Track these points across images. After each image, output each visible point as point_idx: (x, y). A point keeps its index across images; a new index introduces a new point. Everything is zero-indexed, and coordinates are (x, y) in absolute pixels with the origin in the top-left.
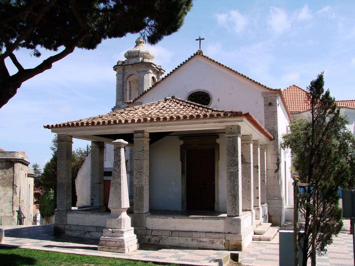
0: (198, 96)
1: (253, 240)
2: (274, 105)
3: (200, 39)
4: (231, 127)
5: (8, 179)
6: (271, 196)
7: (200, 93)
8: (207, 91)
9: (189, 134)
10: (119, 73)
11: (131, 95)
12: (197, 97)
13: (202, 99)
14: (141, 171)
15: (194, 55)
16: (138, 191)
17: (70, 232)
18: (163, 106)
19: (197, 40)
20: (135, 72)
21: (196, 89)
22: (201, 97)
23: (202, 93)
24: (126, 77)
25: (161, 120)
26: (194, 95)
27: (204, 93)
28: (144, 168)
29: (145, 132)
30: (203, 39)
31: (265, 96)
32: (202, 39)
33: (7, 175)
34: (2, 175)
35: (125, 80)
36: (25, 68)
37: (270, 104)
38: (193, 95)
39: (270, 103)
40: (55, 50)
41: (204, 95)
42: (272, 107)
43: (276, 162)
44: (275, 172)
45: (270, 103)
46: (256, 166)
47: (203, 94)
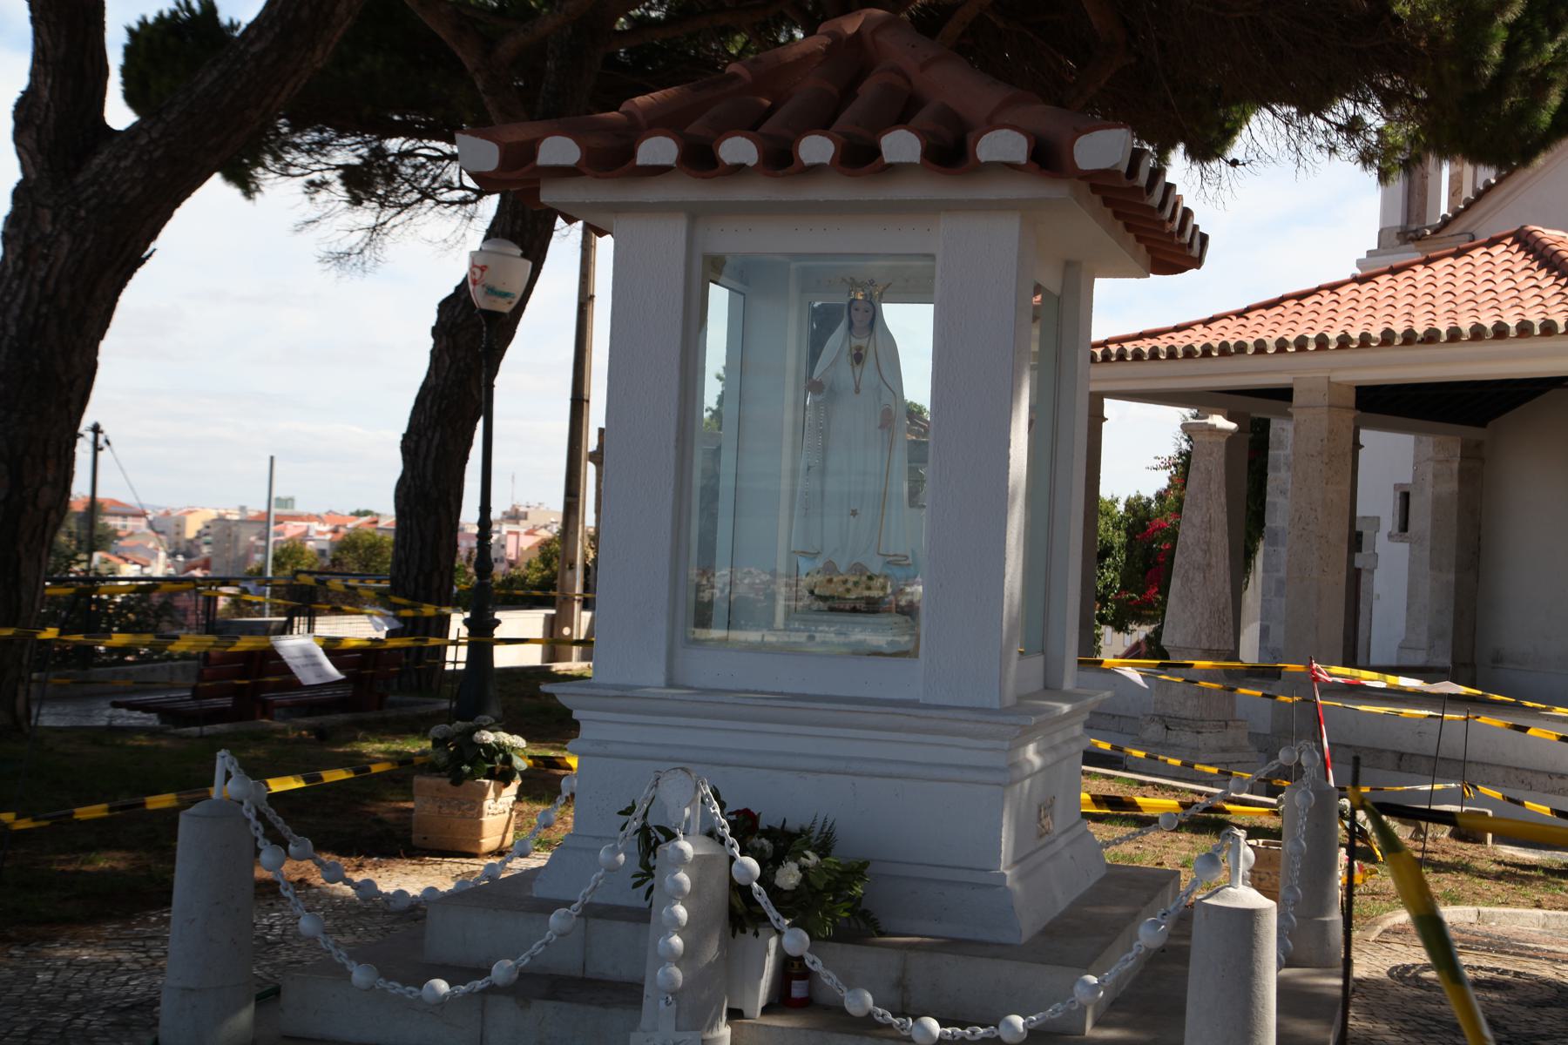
25: (1331, 347)
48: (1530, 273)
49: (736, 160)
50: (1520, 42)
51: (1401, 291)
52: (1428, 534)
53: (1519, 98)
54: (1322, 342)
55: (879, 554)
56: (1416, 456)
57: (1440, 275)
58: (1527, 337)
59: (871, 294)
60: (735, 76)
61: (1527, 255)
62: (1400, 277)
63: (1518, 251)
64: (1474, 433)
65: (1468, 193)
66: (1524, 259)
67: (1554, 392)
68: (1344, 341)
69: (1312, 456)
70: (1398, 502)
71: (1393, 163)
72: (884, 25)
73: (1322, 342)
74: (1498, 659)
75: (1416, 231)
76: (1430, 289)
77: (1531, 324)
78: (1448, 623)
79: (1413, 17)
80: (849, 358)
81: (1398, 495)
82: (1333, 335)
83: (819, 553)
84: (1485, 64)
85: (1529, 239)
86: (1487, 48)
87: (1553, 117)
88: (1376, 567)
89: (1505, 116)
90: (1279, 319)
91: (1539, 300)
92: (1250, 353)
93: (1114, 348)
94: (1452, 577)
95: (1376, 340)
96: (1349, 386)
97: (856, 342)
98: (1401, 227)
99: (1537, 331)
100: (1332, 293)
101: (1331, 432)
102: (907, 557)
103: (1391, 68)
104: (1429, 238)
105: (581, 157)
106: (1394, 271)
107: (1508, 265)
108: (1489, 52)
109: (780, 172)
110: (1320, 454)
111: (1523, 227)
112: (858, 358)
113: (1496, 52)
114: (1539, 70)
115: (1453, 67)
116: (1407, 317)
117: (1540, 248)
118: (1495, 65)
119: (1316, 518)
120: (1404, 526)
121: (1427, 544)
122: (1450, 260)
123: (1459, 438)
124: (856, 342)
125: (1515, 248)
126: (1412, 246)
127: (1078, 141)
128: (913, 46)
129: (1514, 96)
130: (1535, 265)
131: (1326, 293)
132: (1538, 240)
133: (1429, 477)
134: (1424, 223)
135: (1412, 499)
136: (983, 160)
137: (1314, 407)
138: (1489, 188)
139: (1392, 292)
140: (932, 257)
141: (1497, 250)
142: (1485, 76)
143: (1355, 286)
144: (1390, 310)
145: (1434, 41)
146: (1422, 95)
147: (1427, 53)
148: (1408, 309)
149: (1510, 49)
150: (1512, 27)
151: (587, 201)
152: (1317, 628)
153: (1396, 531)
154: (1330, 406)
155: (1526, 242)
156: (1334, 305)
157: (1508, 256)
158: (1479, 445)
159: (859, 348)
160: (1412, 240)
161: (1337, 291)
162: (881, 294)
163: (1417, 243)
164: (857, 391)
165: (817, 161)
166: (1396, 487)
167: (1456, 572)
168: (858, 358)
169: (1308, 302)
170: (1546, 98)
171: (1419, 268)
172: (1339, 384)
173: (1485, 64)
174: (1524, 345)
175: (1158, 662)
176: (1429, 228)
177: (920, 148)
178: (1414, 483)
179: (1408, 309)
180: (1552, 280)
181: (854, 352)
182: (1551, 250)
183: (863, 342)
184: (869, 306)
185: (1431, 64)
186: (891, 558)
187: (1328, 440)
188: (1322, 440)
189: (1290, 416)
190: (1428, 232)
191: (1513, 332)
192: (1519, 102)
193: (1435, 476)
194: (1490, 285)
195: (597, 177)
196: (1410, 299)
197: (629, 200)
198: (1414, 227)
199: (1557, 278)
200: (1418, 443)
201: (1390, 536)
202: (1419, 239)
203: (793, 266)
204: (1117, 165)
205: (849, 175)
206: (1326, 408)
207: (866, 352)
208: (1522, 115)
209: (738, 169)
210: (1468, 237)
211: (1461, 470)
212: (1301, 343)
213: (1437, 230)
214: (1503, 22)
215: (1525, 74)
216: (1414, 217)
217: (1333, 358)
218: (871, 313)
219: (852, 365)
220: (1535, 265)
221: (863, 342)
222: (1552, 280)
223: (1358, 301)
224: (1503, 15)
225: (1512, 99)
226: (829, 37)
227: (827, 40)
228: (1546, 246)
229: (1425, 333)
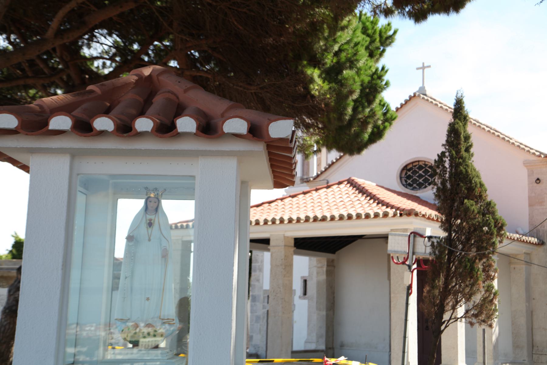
0: (417, 168)
3: (423, 68)
7: (421, 163)
11: (321, 165)
12: (416, 178)
13: (424, 174)
15: (411, 98)
17: (360, 51)
19: (418, 69)
21: (414, 157)
22: (422, 179)
26: (411, 166)
30: (429, 67)
37: (538, 182)
38: (408, 167)
39: (538, 179)
41: (428, 166)
45: (538, 179)
47: (426, 165)
48: (355, 195)
49: (102, 128)
50: (357, 107)
51: (309, 201)
52: (315, 296)
53: (357, 128)
54: (282, 221)
55: (160, 319)
56: (309, 265)
57: (322, 195)
58: (360, 219)
59: (158, 194)
60: (92, 92)
61: (353, 188)
62: (308, 195)
63: (350, 186)
64: (331, 256)
65: (323, 166)
66: (352, 189)
67: (359, 241)
68: (290, 221)
69: (278, 266)
70: (302, 284)
71: (310, 152)
72: (162, 73)
73: (282, 221)
74: (342, 346)
75: (307, 179)
76: (319, 200)
77: (361, 214)
78: (323, 331)
79: (319, 96)
80: (146, 224)
81: (302, 281)
82: (286, 218)
83: (129, 319)
84: (346, 114)
85: (353, 182)
86: (347, 109)
87: (369, 136)
88: (294, 310)
89: (352, 135)
90: (262, 211)
91: (360, 205)
92: (336, 219)
93: (179, 225)
94: (324, 313)
95: (303, 220)
96: (292, 238)
97: (149, 217)
98: (301, 177)
99: (363, 217)
100: (282, 201)
101: (285, 256)
102: (173, 320)
103: (310, 116)
104: (312, 181)
105: (19, 124)
106: (305, 193)
107: (347, 192)
108: (347, 110)
109: (125, 135)
110: (281, 265)
111: (350, 178)
112: (150, 224)
113: (350, 110)
114: (364, 118)
115: (335, 115)
116: (312, 211)
117: (357, 186)
118: (350, 115)
119: (280, 291)
120: (305, 293)
121: (315, 300)
122: (325, 190)
123: (326, 258)
124: (149, 217)
125: (349, 185)
126: (305, 184)
127: (271, 125)
128: (179, 82)
129: (355, 127)
130: (357, 192)
131: (279, 201)
132: (356, 183)
133: (315, 273)
134: (309, 176)
135: (308, 283)
136: (226, 132)
137: (279, 246)
138: (333, 163)
139: (304, 201)
140: (193, 177)
141: (342, 186)
142: (346, 119)
143: (290, 199)
144: (305, 208)
145: (327, 105)
146: (320, 126)
147: (325, 109)
148: (312, 208)
149: (355, 109)
150: (355, 101)
151: (18, 147)
152: (281, 337)
153: (302, 295)
154: (285, 246)
155: (351, 183)
156: (283, 206)
157: (346, 188)
158: (333, 261)
159: (151, 220)
160: (306, 182)
161: (283, 200)
162: (162, 194)
163: (308, 183)
164: (149, 240)
165: (144, 130)
166: (302, 277)
167: (327, 311)
168: (150, 224)
169: (273, 204)
170: (366, 129)
171: (314, 192)
172: (288, 237)
173: (346, 114)
174: (359, 222)
175: (258, 360)
176: (312, 177)
177: (196, 126)
178: (309, 276)
179: (312, 208)
180: (364, 197)
181: (148, 222)
182: (362, 187)
183: (152, 217)
184: (156, 200)
185: (326, 113)
186: (166, 321)
187: (284, 259)
188: (282, 260)
189: (268, 250)
190: (312, 179)
191: (354, 217)
192: (357, 130)
193: (318, 273)
194: (341, 199)
195: (27, 134)
196: (312, 204)
197: (42, 147)
198: (305, 177)
199: (366, 197)
200: (310, 260)
201: (300, 297)
202: (308, 182)
203: (111, 181)
204: (288, 136)
205: (160, 137)
206: (283, 247)
207: (154, 222)
208: (358, 135)
209: (102, 133)
210: (326, 181)
211: (327, 271)
212: (274, 221)
213: (315, 179)
214: (352, 99)
215: (359, 119)
216: (305, 173)
217: (286, 226)
218: (157, 204)
219: (147, 228)
220: (357, 192)
221: (152, 217)
222: (364, 197)
223: (292, 205)
224: (352, 97)
225: (355, 128)
226: (137, 76)
227: (136, 78)
228: (360, 185)
229: (322, 217)
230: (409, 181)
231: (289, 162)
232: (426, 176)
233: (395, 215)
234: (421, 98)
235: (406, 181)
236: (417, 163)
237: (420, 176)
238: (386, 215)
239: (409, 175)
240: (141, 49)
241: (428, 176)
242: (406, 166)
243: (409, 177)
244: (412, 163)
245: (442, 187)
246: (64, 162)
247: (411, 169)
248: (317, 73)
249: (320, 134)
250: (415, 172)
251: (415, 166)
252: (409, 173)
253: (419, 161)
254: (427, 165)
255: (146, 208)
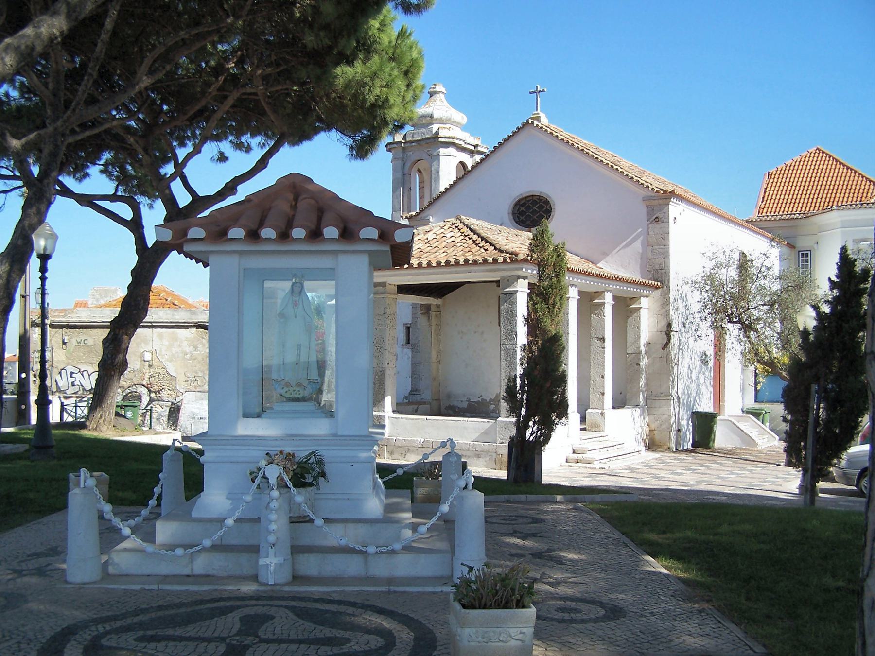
1: (567, 462)
2: (665, 220)
4: (509, 278)
5: (200, 358)
6: (654, 393)
7: (535, 198)
8: (547, 195)
9: (748, 232)
10: (395, 158)
14: (381, 346)
16: (377, 377)
18: (443, 235)
20: (425, 156)
23: (538, 197)
24: (408, 165)
26: (524, 201)
27: (541, 198)
28: (387, 341)
29: (387, 284)
31: (648, 203)
32: (534, 93)
33: (198, 352)
34: (191, 352)
35: (406, 171)
36: (201, 194)
38: (521, 203)
40: (36, 402)
42: (661, 225)
43: (665, 329)
44: (663, 349)
46: (602, 337)
112: (296, 304)
120: (408, 342)
164: (296, 317)
209: (268, 240)
221: (298, 298)
230: (522, 218)
231: (567, 496)
232: (541, 213)
233: (505, 261)
234: (535, 125)
235: (518, 217)
236: (531, 198)
237: (534, 212)
238: (495, 261)
239: (523, 211)
240: (809, 342)
241: (543, 212)
242: (519, 201)
243: (521, 213)
244: (526, 197)
245: (862, 315)
246: (234, 260)
247: (524, 204)
248: (107, 513)
249: (149, 101)
250: (528, 208)
251: (529, 201)
252: (523, 209)
253: (532, 196)
254: (542, 200)
255: (292, 291)
